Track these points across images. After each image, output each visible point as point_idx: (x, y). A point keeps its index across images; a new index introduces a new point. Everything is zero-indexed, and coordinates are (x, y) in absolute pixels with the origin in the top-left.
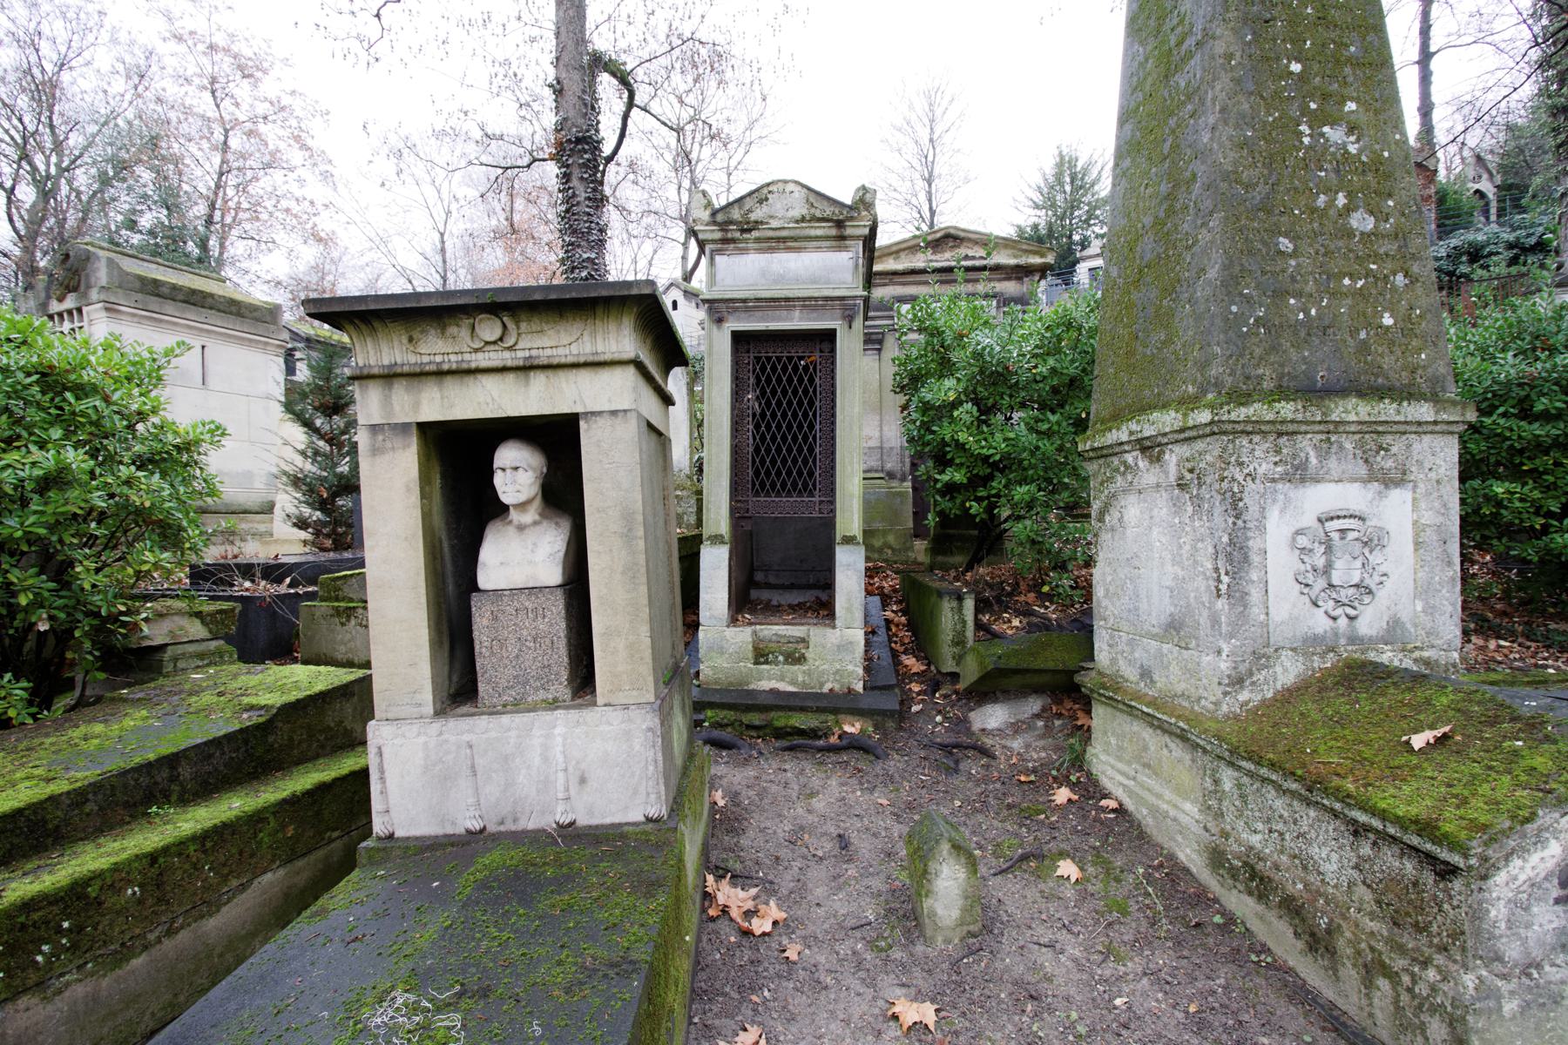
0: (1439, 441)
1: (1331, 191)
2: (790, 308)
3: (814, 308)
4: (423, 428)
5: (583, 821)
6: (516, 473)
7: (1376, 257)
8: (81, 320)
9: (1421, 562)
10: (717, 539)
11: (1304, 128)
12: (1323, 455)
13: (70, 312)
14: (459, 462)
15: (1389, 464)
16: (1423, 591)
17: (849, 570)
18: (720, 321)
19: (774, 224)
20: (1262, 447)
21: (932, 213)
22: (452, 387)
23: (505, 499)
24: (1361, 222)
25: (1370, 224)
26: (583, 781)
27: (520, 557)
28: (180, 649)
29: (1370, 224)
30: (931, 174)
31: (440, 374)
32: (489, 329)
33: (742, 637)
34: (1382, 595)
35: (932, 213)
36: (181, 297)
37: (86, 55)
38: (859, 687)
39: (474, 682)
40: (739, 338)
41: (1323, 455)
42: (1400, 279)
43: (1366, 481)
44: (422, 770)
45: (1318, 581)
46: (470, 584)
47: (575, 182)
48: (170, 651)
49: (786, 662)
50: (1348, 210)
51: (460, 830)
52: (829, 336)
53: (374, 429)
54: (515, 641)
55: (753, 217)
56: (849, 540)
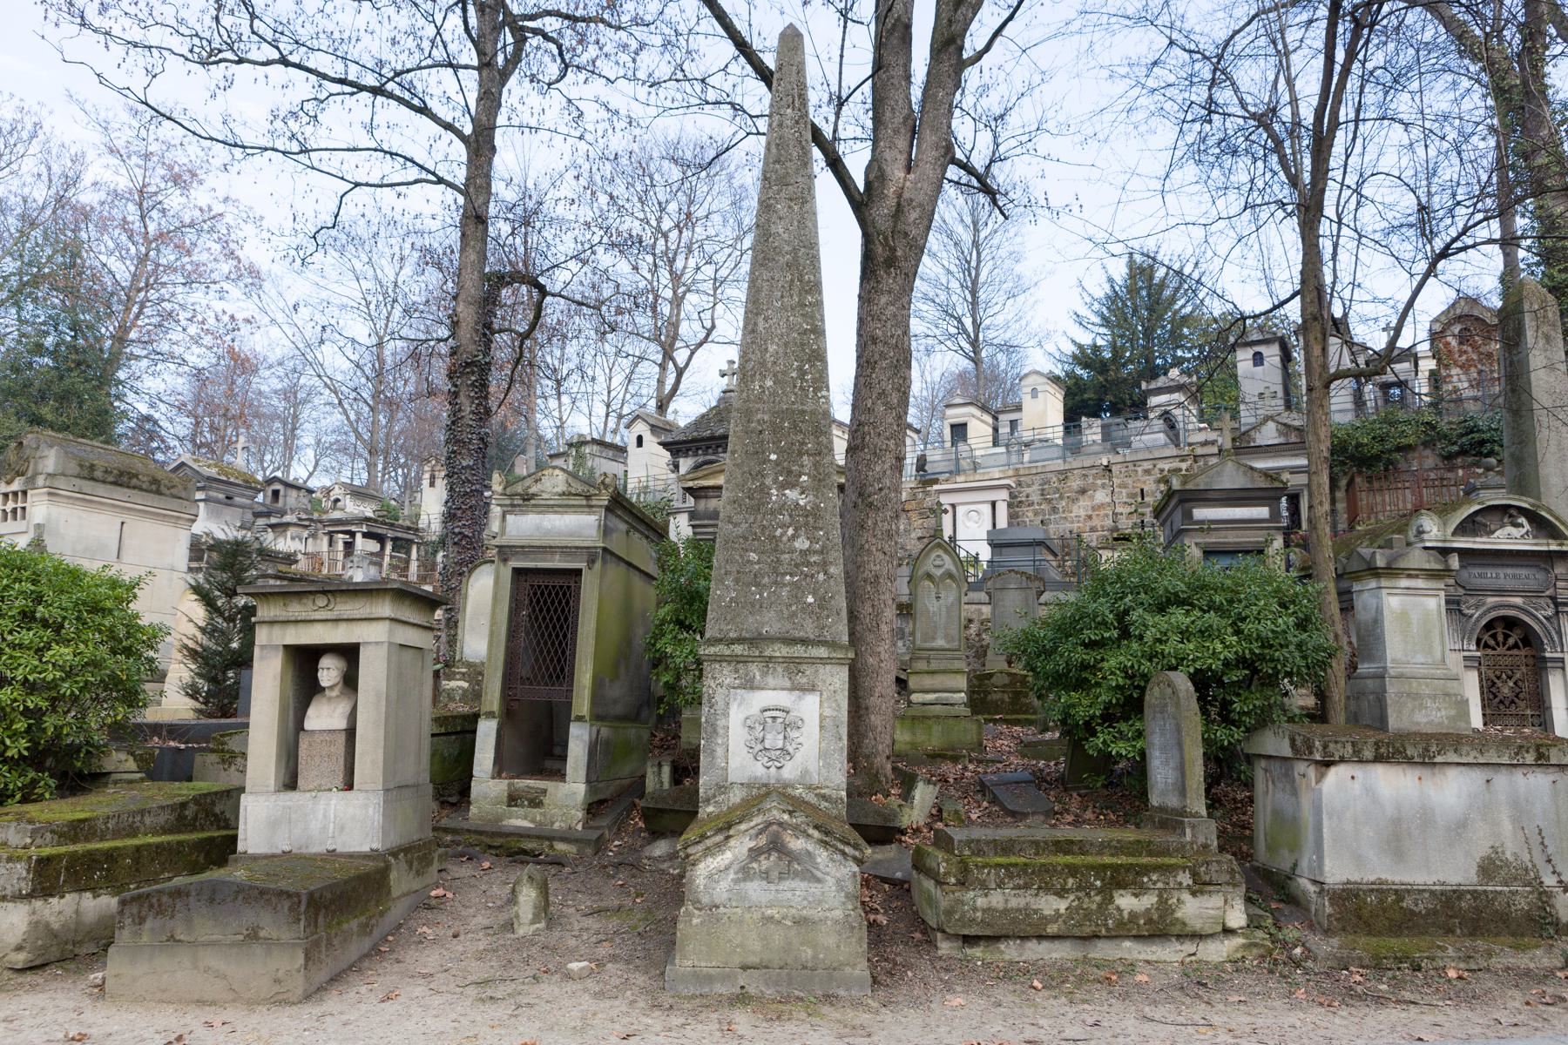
0: (836, 669)
1: (784, 526)
2: (553, 553)
3: (569, 554)
4: (286, 647)
5: (340, 849)
6: (329, 672)
7: (808, 564)
8: (25, 501)
9: (822, 739)
10: (490, 715)
11: (774, 491)
12: (764, 674)
13: (15, 494)
14: (304, 660)
15: (805, 680)
16: (823, 754)
17: (579, 740)
18: (505, 560)
19: (545, 496)
20: (727, 669)
21: (977, 326)
22: (302, 629)
23: (323, 684)
24: (802, 544)
25: (807, 544)
26: (342, 829)
27: (324, 717)
28: (118, 776)
29: (807, 544)
30: (975, 282)
31: (297, 622)
32: (321, 601)
33: (500, 787)
34: (799, 757)
35: (977, 326)
36: (111, 479)
37: (14, 167)
38: (579, 827)
39: (296, 782)
40: (517, 572)
41: (764, 674)
42: (821, 577)
43: (792, 689)
44: (266, 822)
45: (759, 749)
46: (299, 726)
47: (462, 399)
48: (114, 777)
49: (530, 806)
50: (794, 537)
51: (279, 851)
52: (578, 572)
53: (262, 647)
54: (318, 763)
55: (531, 491)
56: (580, 719)
